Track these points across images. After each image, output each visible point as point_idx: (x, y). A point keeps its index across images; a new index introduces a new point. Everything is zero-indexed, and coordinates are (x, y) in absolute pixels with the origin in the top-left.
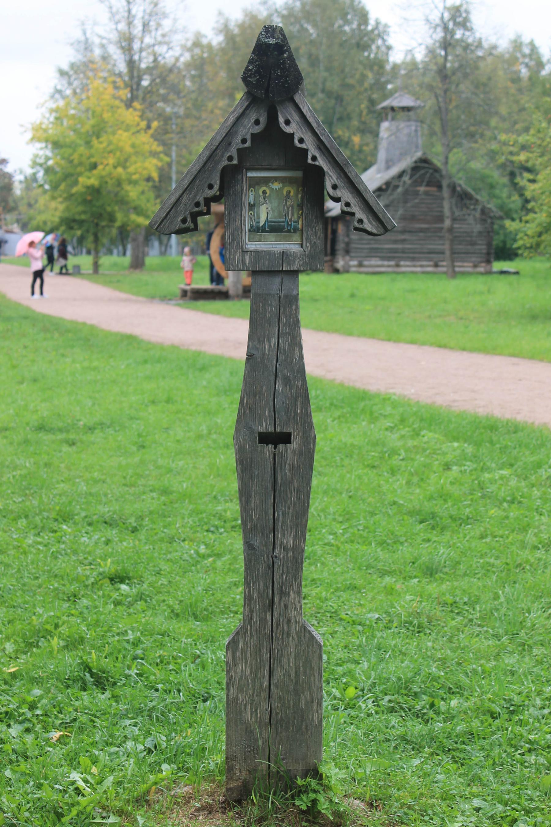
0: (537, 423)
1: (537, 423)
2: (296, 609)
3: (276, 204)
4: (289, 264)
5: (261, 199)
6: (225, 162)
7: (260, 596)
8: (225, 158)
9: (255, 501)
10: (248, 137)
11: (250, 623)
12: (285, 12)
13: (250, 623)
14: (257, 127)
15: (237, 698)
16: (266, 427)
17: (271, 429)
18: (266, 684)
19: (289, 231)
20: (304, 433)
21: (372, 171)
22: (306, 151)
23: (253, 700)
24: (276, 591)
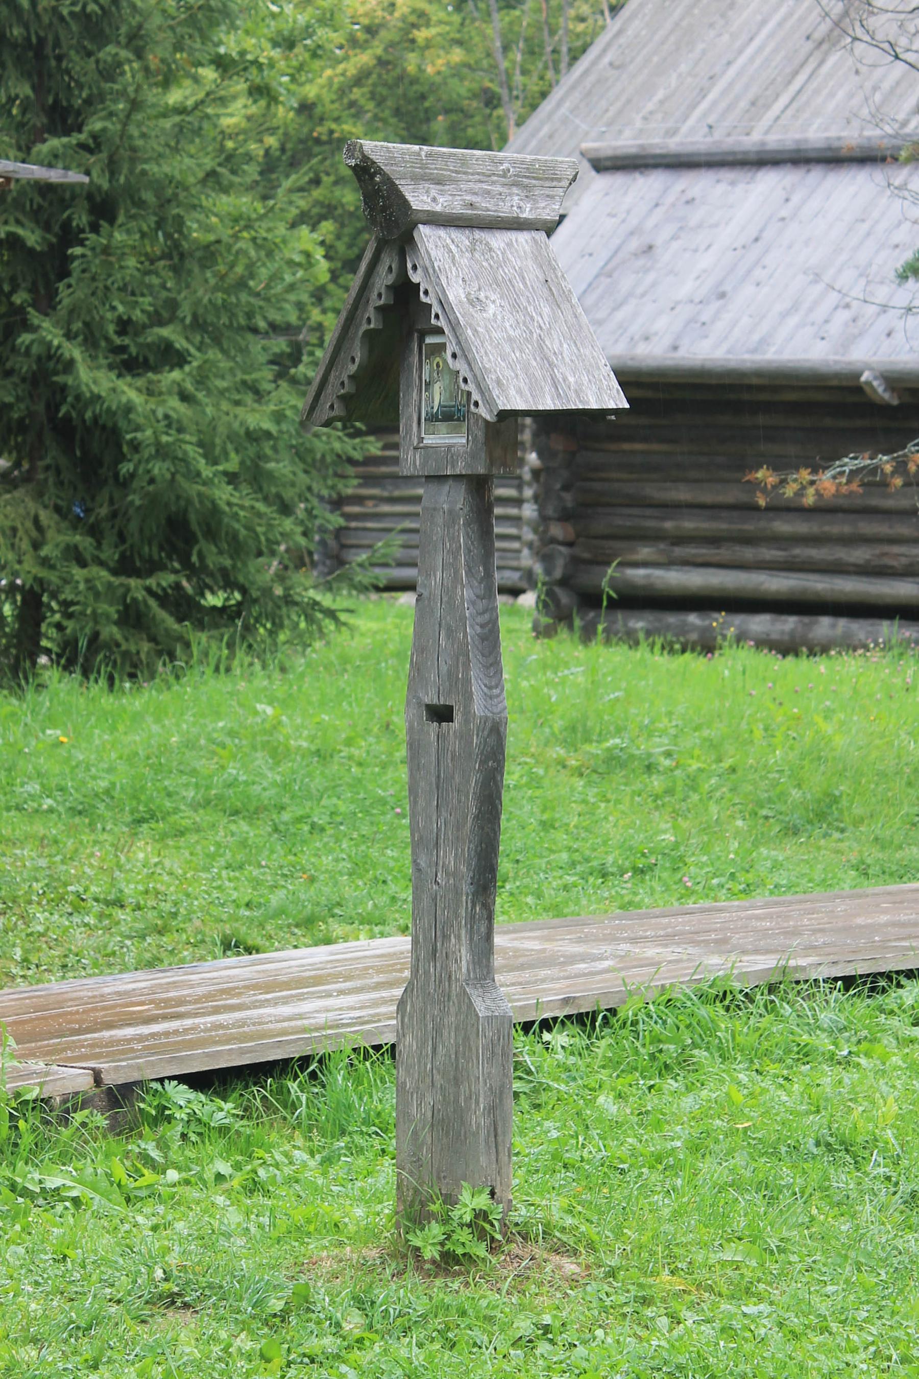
0: (766, 651)
1: (766, 651)
2: (456, 961)
3: (447, 382)
4: (453, 467)
5: (435, 375)
6: (364, 327)
7: (425, 939)
8: (364, 321)
9: (421, 803)
10: (383, 291)
11: (416, 976)
12: (220, 70)
13: (416, 976)
14: (390, 277)
15: (405, 1083)
16: (430, 698)
17: (435, 701)
18: (429, 1066)
19: (458, 420)
20: (465, 708)
21: (277, 350)
22: (378, 309)
23: (418, 1088)
24: (438, 933)
